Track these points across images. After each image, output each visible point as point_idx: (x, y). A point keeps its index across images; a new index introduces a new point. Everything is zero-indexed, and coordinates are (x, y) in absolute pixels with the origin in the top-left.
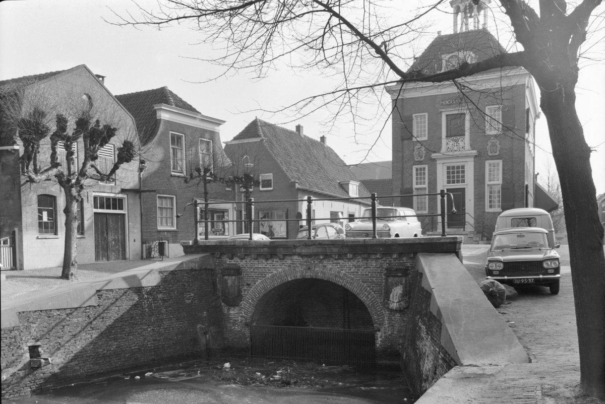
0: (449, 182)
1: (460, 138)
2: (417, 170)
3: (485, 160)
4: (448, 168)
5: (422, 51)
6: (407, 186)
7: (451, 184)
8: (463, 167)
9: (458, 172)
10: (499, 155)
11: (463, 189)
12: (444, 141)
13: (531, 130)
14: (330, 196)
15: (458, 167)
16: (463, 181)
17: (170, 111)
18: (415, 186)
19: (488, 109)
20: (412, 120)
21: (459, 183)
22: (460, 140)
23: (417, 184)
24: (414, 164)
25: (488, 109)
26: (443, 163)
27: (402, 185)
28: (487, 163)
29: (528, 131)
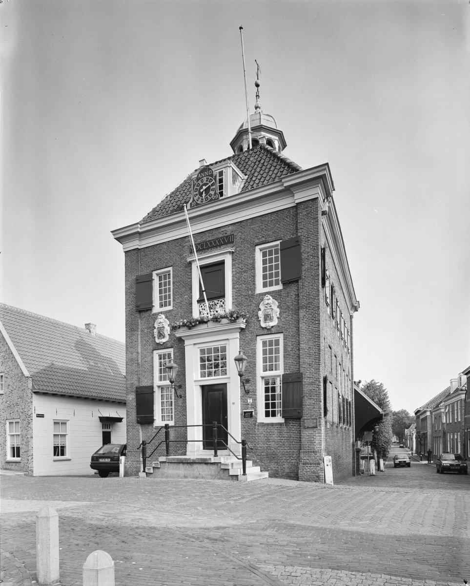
0: (203, 375)
6: (145, 383)
10: (278, 326)
18: (157, 382)
20: (151, 280)
22: (218, 305)
26: (195, 344)
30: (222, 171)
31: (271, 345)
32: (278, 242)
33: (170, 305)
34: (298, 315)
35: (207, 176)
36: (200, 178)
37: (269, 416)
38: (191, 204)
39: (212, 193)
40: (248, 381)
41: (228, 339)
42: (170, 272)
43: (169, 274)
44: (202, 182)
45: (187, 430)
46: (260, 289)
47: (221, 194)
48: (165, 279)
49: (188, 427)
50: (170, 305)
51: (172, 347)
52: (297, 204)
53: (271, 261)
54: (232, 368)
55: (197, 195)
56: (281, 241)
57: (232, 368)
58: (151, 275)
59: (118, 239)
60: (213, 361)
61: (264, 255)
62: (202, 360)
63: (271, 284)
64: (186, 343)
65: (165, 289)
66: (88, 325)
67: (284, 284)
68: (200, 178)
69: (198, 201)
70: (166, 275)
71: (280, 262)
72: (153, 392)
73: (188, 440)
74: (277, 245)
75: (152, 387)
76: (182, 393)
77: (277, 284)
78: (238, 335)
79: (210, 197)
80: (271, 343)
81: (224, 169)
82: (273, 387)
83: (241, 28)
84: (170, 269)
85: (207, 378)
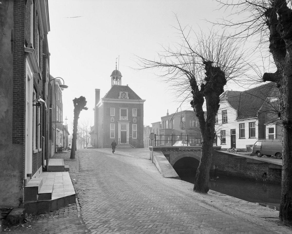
0: (121, 129)
1: (125, 117)
8: (126, 125)
12: (120, 116)
16: (126, 129)
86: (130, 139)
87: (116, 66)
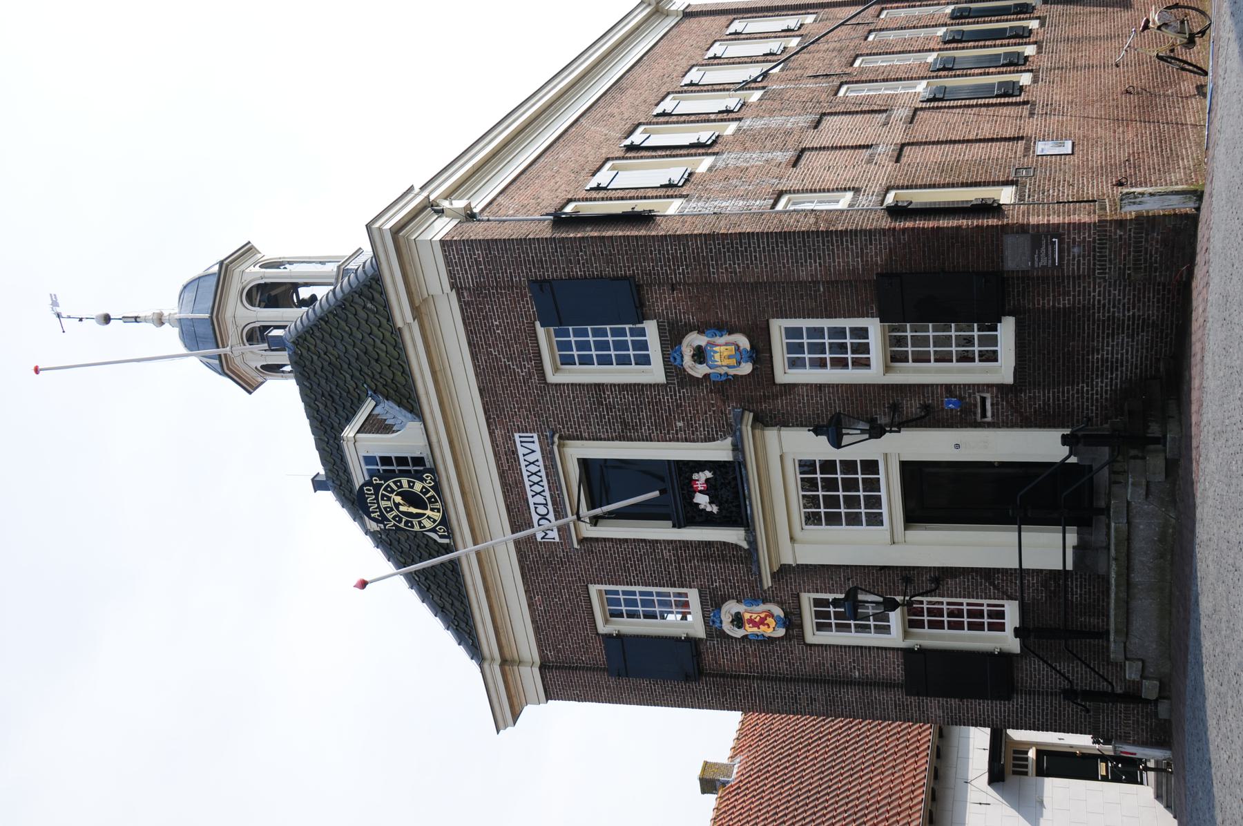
0: (875, 520)
2: (794, 364)
3: (774, 383)
4: (812, 519)
5: (315, 455)
6: (896, 670)
7: (883, 493)
9: (830, 485)
11: (905, 466)
13: (641, 206)
14: (935, 797)
15: (809, 484)
17: (468, 515)
19: (556, 370)
20: (620, 637)
21: (879, 498)
23: (866, 364)
24: (801, 636)
25: (556, 370)
26: (792, 539)
27: (888, 685)
28: (784, 375)
29: (645, 218)
30: (365, 458)
31: (857, 349)
32: (541, 331)
33: (686, 595)
34: (724, 285)
35: (377, 498)
36: (382, 514)
37: (995, 352)
38: (441, 537)
39: (418, 486)
40: (895, 408)
41: (781, 456)
42: (600, 591)
43: (607, 592)
44: (392, 510)
45: (1039, 572)
46: (655, 373)
47: (418, 461)
48: (618, 602)
49: (1024, 567)
50: (686, 595)
51: (798, 596)
52: (453, 286)
53: (621, 346)
54: (859, 449)
55: (420, 523)
56: (538, 324)
57: (859, 449)
58: (608, 637)
59: (515, 717)
60: (835, 494)
61: (568, 361)
62: (833, 519)
63: (644, 346)
64: (787, 559)
65: (644, 603)
66: (708, 785)
67: (642, 318)
68: (382, 514)
69: (435, 521)
70: (611, 600)
71: (608, 327)
72: (923, 651)
73: (1061, 568)
74: (548, 333)
75: (907, 652)
76: (926, 577)
77: (642, 332)
78: (771, 434)
79: (428, 491)
80: (794, 348)
81: (362, 453)
82: (830, 348)
83: (37, 370)
84: (594, 589)
85: (884, 510)
86: (1013, 407)
87: (136, 319)
